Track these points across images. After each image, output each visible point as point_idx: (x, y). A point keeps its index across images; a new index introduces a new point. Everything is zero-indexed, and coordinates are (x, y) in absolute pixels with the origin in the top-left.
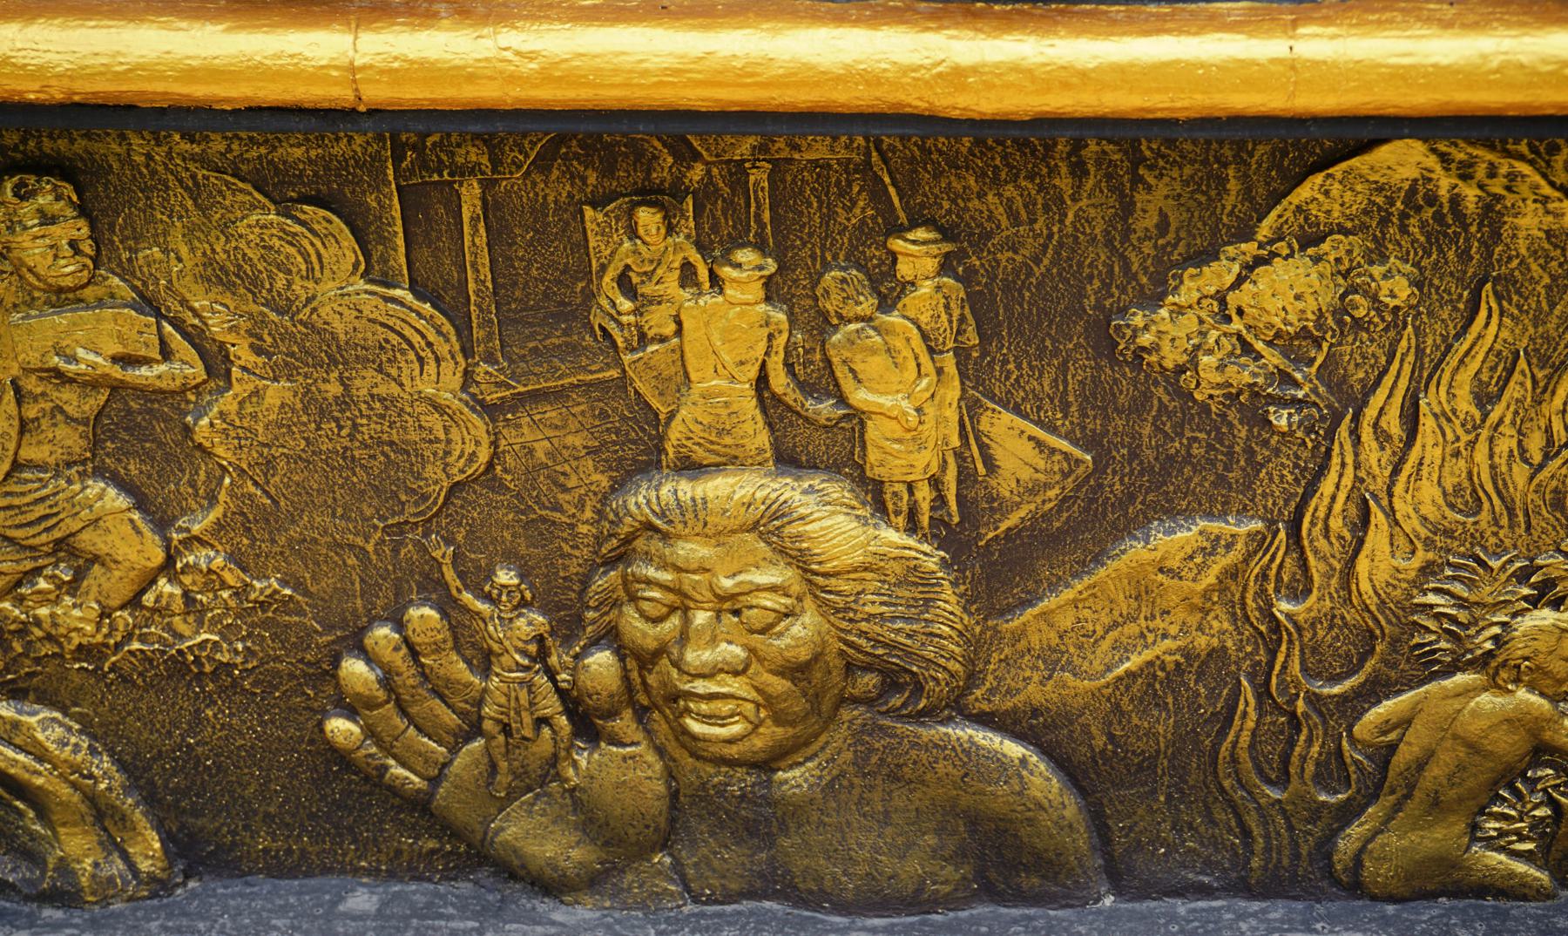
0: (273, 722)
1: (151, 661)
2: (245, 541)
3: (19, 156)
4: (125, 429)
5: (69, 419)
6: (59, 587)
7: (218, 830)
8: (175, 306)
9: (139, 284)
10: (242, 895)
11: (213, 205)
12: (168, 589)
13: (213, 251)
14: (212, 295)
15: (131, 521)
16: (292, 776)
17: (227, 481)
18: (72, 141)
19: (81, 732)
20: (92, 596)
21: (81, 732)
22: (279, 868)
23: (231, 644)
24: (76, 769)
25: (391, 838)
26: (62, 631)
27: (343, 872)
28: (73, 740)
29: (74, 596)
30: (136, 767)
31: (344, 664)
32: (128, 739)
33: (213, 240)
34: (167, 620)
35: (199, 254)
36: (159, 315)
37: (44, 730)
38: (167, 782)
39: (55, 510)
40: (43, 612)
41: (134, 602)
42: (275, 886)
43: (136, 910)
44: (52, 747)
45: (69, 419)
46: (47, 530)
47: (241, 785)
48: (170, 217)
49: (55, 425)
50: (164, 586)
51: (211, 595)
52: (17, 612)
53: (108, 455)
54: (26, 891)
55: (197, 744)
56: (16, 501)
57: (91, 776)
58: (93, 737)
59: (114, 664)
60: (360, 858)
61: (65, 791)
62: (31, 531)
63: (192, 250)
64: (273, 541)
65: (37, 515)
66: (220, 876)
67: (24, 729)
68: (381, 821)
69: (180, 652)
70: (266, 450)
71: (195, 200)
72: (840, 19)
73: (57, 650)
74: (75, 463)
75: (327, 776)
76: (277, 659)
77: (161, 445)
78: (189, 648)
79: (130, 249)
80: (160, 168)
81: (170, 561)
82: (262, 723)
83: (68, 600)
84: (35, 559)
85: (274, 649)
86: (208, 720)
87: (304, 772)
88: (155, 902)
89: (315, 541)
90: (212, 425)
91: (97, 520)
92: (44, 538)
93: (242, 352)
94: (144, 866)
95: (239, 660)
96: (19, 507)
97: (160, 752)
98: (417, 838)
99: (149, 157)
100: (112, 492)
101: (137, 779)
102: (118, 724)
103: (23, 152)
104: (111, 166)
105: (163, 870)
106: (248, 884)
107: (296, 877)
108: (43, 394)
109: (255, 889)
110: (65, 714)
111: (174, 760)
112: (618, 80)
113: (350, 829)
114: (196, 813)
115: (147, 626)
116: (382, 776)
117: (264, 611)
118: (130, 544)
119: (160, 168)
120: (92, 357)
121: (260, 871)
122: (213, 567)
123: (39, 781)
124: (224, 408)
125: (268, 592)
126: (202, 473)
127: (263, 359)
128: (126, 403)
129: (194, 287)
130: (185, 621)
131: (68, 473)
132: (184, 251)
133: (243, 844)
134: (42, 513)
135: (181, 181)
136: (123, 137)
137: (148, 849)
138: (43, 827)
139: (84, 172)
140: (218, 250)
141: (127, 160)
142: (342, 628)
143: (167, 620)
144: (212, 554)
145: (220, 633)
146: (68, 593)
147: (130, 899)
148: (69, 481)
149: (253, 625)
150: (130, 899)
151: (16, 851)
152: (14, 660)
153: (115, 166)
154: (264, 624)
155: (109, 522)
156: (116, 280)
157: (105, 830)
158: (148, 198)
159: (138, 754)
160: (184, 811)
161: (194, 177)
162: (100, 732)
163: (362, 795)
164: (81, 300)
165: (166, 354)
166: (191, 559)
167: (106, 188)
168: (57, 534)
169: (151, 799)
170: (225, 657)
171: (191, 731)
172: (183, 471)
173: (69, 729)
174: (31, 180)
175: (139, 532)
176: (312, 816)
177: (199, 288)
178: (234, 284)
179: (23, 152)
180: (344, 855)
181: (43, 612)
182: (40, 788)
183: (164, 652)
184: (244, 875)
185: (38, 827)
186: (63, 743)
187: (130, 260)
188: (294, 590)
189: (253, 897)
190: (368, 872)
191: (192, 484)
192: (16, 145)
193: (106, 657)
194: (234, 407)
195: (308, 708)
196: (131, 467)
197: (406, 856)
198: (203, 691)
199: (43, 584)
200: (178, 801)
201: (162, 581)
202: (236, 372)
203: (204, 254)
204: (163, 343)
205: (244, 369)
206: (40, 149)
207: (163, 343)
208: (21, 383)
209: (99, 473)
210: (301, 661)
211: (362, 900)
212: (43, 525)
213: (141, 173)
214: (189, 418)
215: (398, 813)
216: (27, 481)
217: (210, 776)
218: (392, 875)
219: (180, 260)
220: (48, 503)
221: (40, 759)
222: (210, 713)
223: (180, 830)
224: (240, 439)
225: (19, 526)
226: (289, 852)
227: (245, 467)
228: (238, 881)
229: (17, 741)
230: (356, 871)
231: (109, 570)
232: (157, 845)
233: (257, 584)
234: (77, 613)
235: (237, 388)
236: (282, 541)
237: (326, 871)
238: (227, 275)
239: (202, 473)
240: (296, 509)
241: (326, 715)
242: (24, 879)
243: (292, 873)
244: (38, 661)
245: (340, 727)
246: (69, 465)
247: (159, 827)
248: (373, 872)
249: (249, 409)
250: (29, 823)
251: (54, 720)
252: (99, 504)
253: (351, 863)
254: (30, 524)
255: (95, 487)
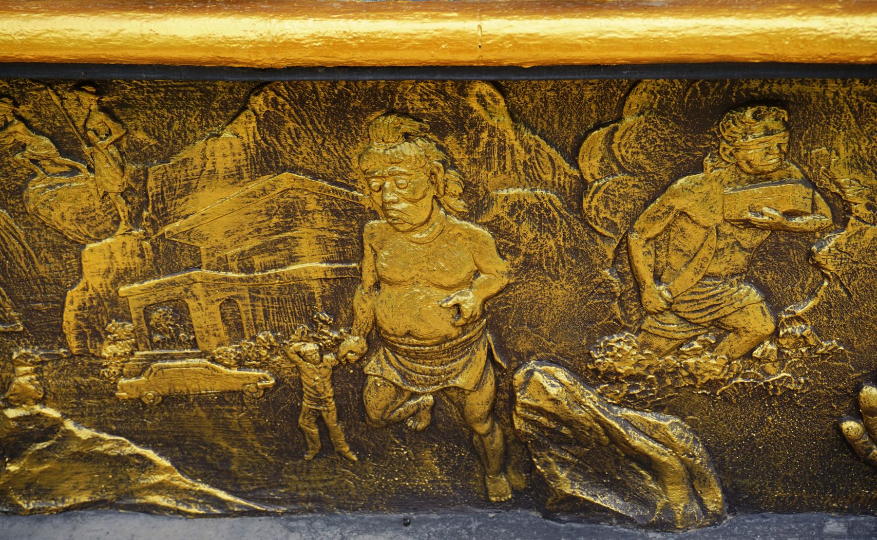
0: (806, 424)
1: (745, 388)
2: (825, 319)
3: (756, 94)
4: (771, 255)
5: (743, 249)
6: (704, 347)
7: (754, 485)
8: (826, 181)
9: (806, 169)
10: (762, 524)
11: (867, 122)
12: (770, 347)
13: (860, 148)
14: (852, 175)
15: (762, 308)
16: (809, 455)
17: (826, 283)
18: (791, 85)
19: (690, 430)
20: (724, 352)
21: (690, 430)
22: (782, 508)
23: (797, 379)
24: (686, 452)
25: (856, 490)
26: (700, 372)
27: (821, 510)
28: (686, 435)
29: (711, 352)
30: (716, 450)
31: (864, 390)
32: (716, 434)
33: (861, 142)
34: (762, 365)
35: (850, 150)
36: (815, 187)
37: (672, 430)
38: (732, 458)
39: (720, 302)
40: (691, 361)
41: (749, 355)
42: (779, 518)
43: (703, 533)
44: (675, 439)
45: (743, 249)
46: (710, 314)
47: (775, 459)
48: (838, 129)
49: (732, 252)
50: (769, 346)
51: (794, 351)
52: (675, 362)
53: (756, 270)
54: (639, 522)
55: (757, 437)
56: (697, 297)
57: (693, 456)
58: (697, 433)
59: (723, 391)
60: (833, 502)
61: (677, 465)
62: (700, 314)
63: (847, 149)
64: (842, 318)
65: (707, 305)
66: (746, 512)
67: (661, 430)
68: (853, 480)
69: (766, 384)
70: (854, 266)
71: (856, 119)
72: (242, 12)
73: (692, 383)
74: (737, 274)
75: (829, 454)
76: (822, 387)
77: (790, 262)
78: (773, 382)
79: (808, 149)
80: (841, 101)
81: (776, 333)
82: (800, 424)
83: (708, 354)
84: (696, 330)
85: (822, 381)
86: (768, 423)
87: (816, 452)
88: (712, 528)
89: (867, 318)
90: (830, 251)
91: (742, 308)
92: (708, 318)
93: (860, 209)
94: (711, 507)
95: (800, 388)
96: (697, 300)
97: (733, 441)
98: (871, 490)
99: (836, 93)
100: (754, 291)
101: (714, 457)
102: (713, 425)
103: (760, 93)
104: (811, 100)
105: (721, 509)
106: (763, 517)
107: (792, 513)
108: (731, 234)
109: (768, 520)
110: (683, 420)
111: (739, 446)
112: (70, 45)
113: (833, 485)
114: (743, 476)
115: (749, 369)
116: (868, 454)
117: (823, 359)
118: (759, 322)
119: (841, 101)
120: (773, 212)
121: (771, 509)
122: (805, 334)
123: (665, 459)
124: (839, 241)
125: (831, 348)
126: (810, 279)
127: (871, 212)
128: (778, 239)
129: (843, 170)
130: (773, 366)
131: (731, 280)
132: (842, 150)
133: (766, 494)
134: (712, 304)
135: (851, 108)
136: (824, 82)
137: (714, 498)
138: (656, 485)
139: (793, 103)
140: (863, 147)
141: (822, 96)
142: (867, 369)
143: (762, 365)
144: (803, 326)
145: (793, 373)
146: (708, 350)
147: (700, 526)
148: (731, 285)
149: (814, 367)
150: (700, 526)
151: (635, 499)
152: (664, 389)
153: (814, 99)
154: (820, 367)
155: (750, 309)
156: (794, 167)
157: (693, 486)
158: (828, 118)
159: (719, 443)
160: (737, 475)
161: (860, 105)
162: (700, 430)
163: (847, 465)
164: (769, 179)
165: (814, 208)
166: (790, 330)
167: (804, 112)
168: (716, 316)
169: (720, 469)
170: (792, 387)
171: (756, 429)
172: (798, 278)
173: (684, 429)
174: (764, 108)
175: (764, 315)
176: (813, 477)
177: (845, 171)
178: (866, 168)
179: (760, 93)
180: (825, 500)
181: (691, 361)
182: (664, 463)
183: (755, 384)
184: (762, 511)
185: (652, 485)
186: (681, 437)
187: (806, 155)
188: (845, 347)
189: (769, 525)
190: (836, 510)
191: (802, 286)
192: (757, 88)
193: (719, 386)
194: (844, 241)
195: (831, 416)
196: (768, 276)
197: (862, 500)
198: (770, 405)
199: (696, 345)
200: (735, 469)
201: (767, 343)
202: (852, 220)
203: (854, 150)
204: (813, 203)
205: (857, 218)
206: (770, 90)
207: (813, 203)
208: (720, 228)
209: (748, 281)
210: (836, 388)
211: (833, 526)
212: (710, 311)
213: (828, 104)
214: (814, 248)
215: (865, 475)
216: (707, 285)
217: (759, 455)
218: (851, 512)
219: (838, 154)
220: (717, 298)
221: (666, 446)
222: (770, 418)
223: (731, 486)
224: (841, 259)
225: (693, 312)
226: (792, 498)
227: (839, 275)
228: (756, 515)
229: (656, 436)
230: (829, 509)
231: (740, 336)
232: (720, 496)
233: (825, 344)
234: (713, 361)
235: (850, 228)
236: (847, 318)
237: (811, 509)
238: (864, 162)
239: (810, 279)
240: (861, 299)
241: (841, 420)
242: (639, 516)
243: (790, 511)
244: (677, 390)
245: (851, 426)
246: (733, 275)
247: (721, 483)
248: (839, 510)
249: (853, 241)
250: (647, 483)
251: (677, 423)
252: (747, 298)
253: (827, 505)
254: (701, 310)
255: (745, 288)
